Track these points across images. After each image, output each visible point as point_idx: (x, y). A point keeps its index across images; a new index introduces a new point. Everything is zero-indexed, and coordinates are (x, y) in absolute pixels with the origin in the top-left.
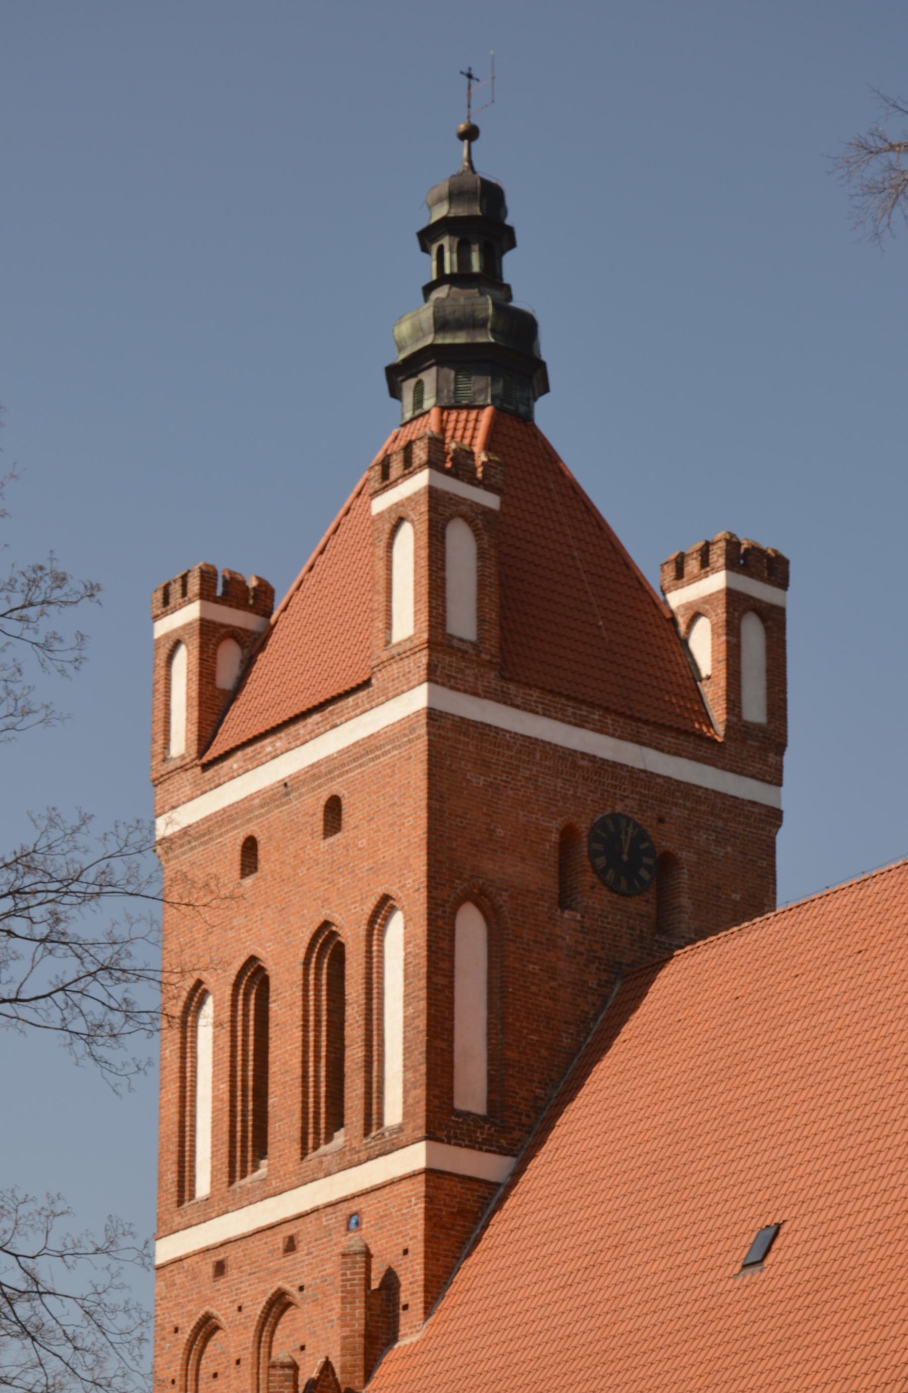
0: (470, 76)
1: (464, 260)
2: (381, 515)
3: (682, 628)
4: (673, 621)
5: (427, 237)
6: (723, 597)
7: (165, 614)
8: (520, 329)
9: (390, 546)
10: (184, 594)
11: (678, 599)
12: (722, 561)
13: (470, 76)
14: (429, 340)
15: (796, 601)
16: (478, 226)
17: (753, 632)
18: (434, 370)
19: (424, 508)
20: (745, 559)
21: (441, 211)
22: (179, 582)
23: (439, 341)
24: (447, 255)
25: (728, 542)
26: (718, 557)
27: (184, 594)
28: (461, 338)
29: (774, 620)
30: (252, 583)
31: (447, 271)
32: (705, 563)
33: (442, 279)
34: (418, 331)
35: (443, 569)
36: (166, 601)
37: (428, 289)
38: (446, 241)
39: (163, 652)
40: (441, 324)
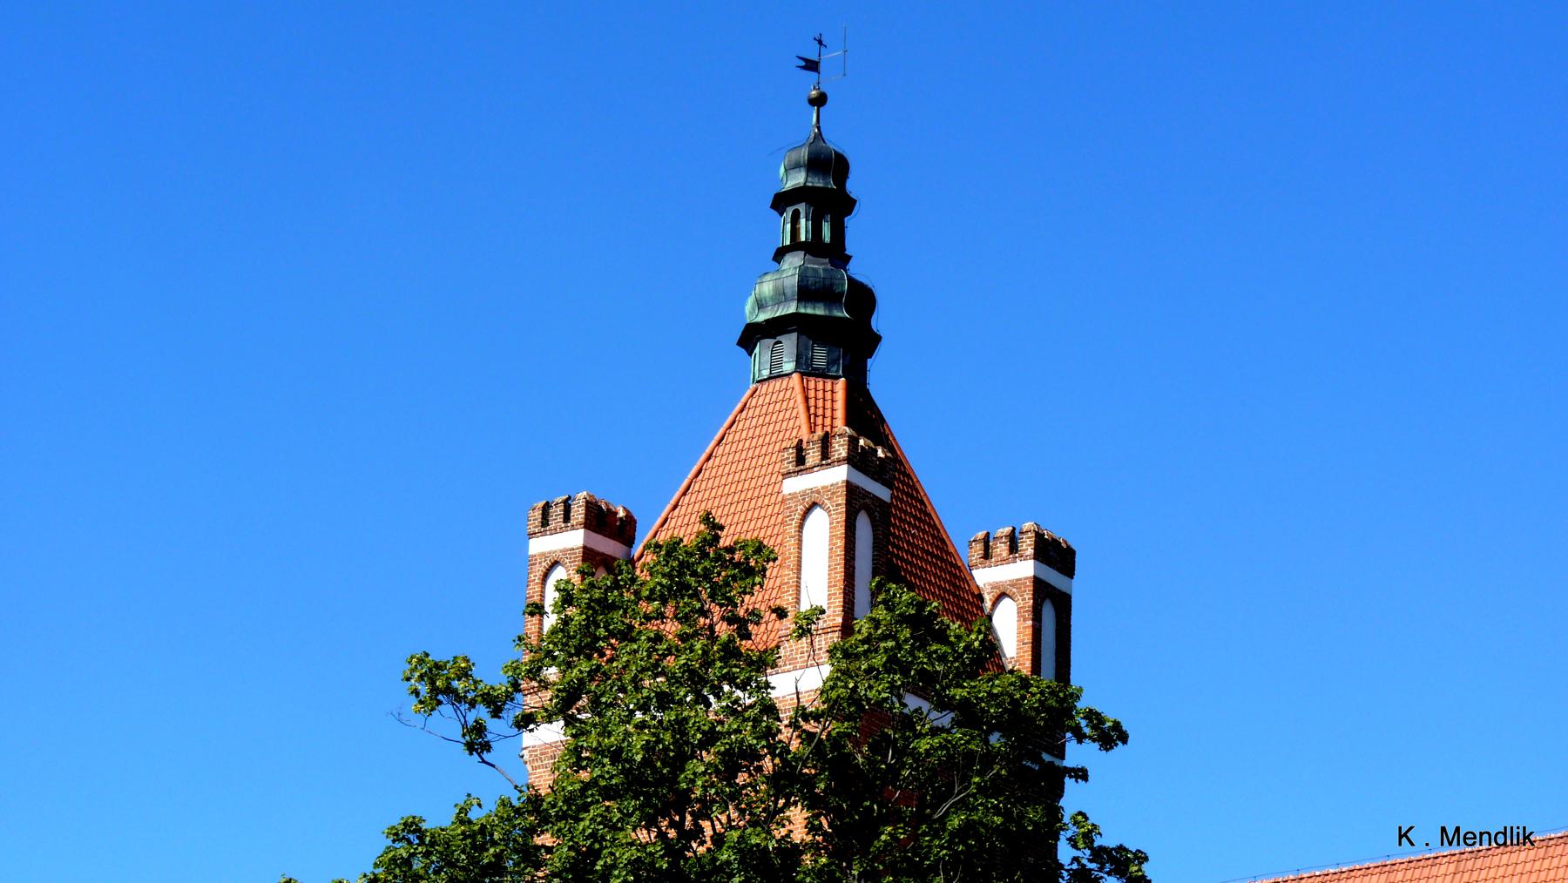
0: (820, 42)
1: (817, 230)
2: (793, 496)
3: (988, 604)
4: (980, 598)
5: (781, 201)
6: (1029, 584)
7: (543, 534)
8: (863, 299)
9: (801, 527)
10: (567, 518)
11: (985, 577)
12: (1030, 551)
13: (820, 42)
14: (791, 308)
15: (1080, 589)
16: (825, 193)
17: (1048, 612)
18: (795, 335)
19: (842, 500)
20: (1055, 555)
21: (798, 179)
22: (561, 507)
23: (802, 311)
24: (803, 221)
25: (1037, 534)
26: (1027, 545)
27: (567, 518)
28: (820, 311)
29: (1063, 604)
30: (621, 514)
31: (803, 239)
32: (1013, 547)
33: (796, 245)
34: (780, 297)
35: (853, 559)
36: (545, 522)
37: (780, 254)
38: (802, 207)
39: (539, 570)
40: (806, 292)
